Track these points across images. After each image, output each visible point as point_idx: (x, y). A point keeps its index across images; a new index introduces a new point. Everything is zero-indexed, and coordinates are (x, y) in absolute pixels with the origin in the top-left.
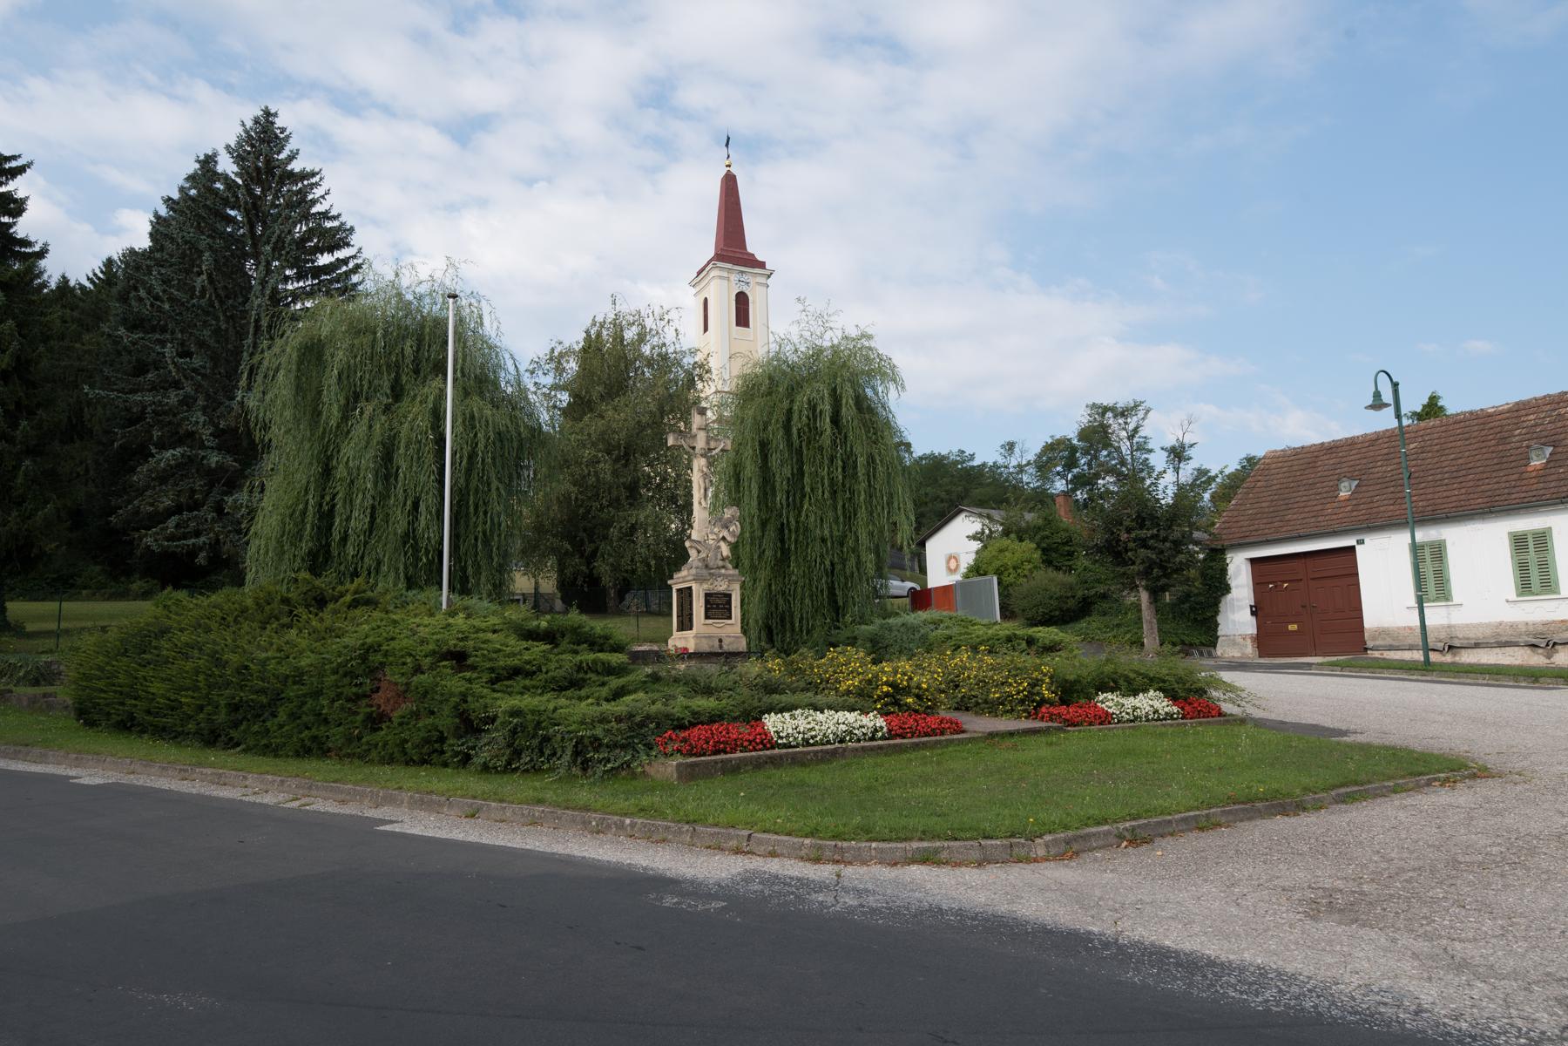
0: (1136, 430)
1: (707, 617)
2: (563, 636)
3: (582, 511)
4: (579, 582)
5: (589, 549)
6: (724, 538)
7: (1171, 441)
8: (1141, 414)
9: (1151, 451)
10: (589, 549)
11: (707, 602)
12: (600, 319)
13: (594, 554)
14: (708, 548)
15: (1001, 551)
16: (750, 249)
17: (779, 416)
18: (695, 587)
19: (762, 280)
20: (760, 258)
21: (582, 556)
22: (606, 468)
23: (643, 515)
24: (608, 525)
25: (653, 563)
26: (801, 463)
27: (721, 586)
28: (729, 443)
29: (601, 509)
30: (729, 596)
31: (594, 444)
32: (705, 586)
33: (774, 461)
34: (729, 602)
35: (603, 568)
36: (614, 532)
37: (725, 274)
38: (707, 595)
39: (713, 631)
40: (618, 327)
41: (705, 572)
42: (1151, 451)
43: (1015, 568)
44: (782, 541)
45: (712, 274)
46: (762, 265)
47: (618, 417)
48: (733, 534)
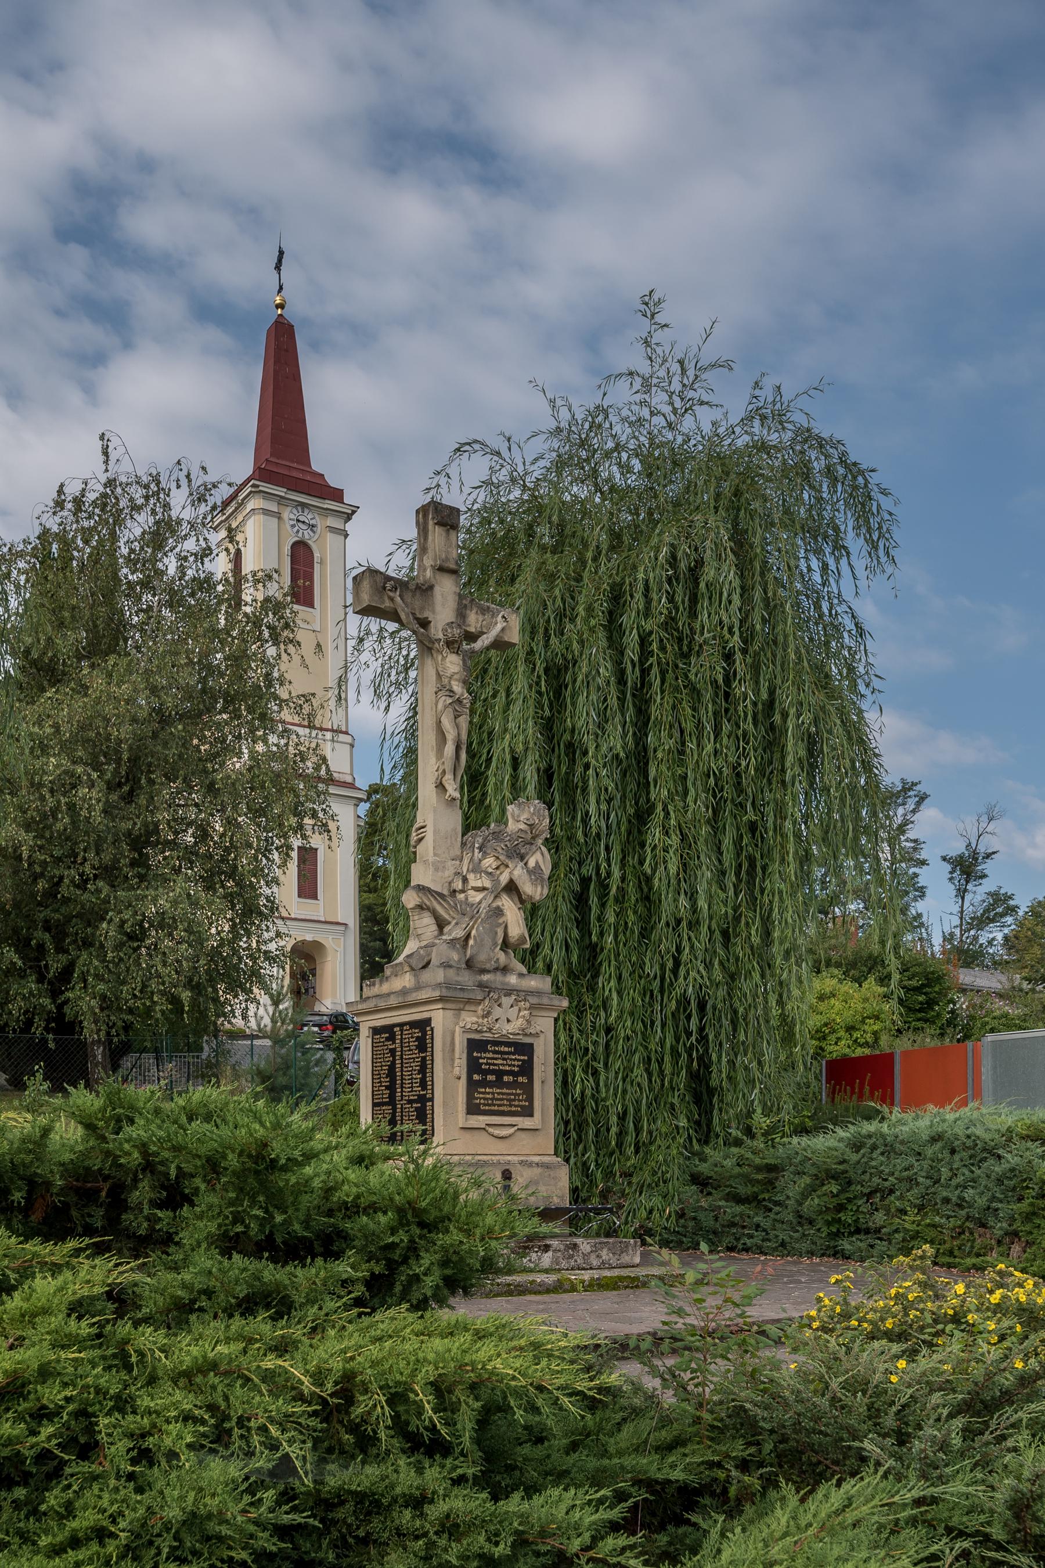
0: (902, 829)
1: (473, 1109)
2: (175, 1196)
3: (41, 885)
4: (38, 1029)
5: (55, 964)
6: (511, 888)
7: (957, 848)
8: (911, 805)
9: (923, 863)
10: (55, 964)
11: (473, 1066)
12: (73, 489)
13: (66, 974)
14: (469, 911)
15: (822, 998)
16: (316, 466)
17: (591, 594)
18: (440, 1019)
19: (337, 523)
20: (333, 482)
21: (40, 980)
22: (91, 797)
23: (157, 902)
24: (95, 916)
25: (186, 995)
26: (642, 720)
27: (509, 1021)
28: (515, 622)
29: (82, 885)
30: (527, 1049)
31: (66, 748)
32: (469, 1019)
33: (583, 714)
34: (527, 1069)
35: (83, 1002)
36: (108, 931)
37: (273, 507)
38: (475, 1046)
39: (485, 1147)
40: (109, 506)
41: (467, 978)
42: (923, 863)
43: (850, 1029)
44: (582, 924)
45: (250, 505)
46: (337, 495)
47: (116, 695)
48: (535, 873)
